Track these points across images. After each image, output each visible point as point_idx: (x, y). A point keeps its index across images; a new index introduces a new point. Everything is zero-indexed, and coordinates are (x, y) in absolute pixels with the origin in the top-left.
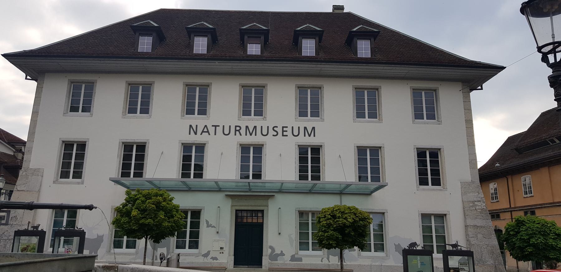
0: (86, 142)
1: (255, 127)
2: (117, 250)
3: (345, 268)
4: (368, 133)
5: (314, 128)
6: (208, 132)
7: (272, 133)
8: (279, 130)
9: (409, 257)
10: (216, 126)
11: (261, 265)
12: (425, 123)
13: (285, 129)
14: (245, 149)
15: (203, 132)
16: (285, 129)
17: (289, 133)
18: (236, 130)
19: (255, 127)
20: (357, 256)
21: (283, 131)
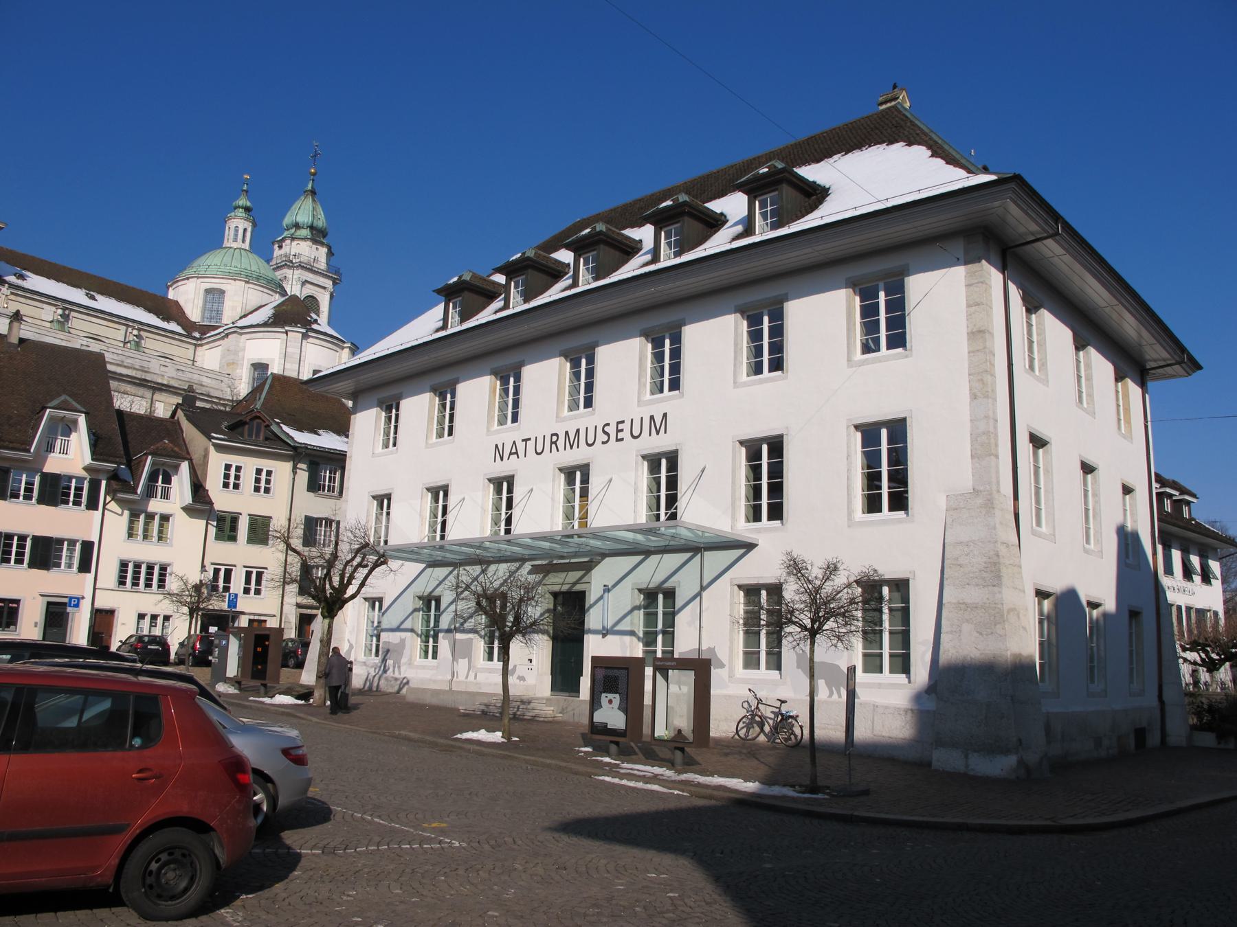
0: (781, 436)
1: (578, 431)
2: (752, 673)
3: (512, 692)
4: (884, 386)
5: (665, 415)
6: (516, 453)
7: (602, 437)
8: (611, 430)
9: (690, 676)
10: (525, 440)
11: (578, 691)
12: (887, 359)
13: (620, 427)
14: (569, 473)
15: (511, 454)
16: (620, 427)
17: (625, 435)
18: (552, 443)
19: (578, 431)
20: (726, 679)
21: (618, 431)
